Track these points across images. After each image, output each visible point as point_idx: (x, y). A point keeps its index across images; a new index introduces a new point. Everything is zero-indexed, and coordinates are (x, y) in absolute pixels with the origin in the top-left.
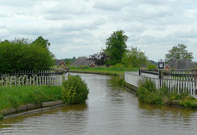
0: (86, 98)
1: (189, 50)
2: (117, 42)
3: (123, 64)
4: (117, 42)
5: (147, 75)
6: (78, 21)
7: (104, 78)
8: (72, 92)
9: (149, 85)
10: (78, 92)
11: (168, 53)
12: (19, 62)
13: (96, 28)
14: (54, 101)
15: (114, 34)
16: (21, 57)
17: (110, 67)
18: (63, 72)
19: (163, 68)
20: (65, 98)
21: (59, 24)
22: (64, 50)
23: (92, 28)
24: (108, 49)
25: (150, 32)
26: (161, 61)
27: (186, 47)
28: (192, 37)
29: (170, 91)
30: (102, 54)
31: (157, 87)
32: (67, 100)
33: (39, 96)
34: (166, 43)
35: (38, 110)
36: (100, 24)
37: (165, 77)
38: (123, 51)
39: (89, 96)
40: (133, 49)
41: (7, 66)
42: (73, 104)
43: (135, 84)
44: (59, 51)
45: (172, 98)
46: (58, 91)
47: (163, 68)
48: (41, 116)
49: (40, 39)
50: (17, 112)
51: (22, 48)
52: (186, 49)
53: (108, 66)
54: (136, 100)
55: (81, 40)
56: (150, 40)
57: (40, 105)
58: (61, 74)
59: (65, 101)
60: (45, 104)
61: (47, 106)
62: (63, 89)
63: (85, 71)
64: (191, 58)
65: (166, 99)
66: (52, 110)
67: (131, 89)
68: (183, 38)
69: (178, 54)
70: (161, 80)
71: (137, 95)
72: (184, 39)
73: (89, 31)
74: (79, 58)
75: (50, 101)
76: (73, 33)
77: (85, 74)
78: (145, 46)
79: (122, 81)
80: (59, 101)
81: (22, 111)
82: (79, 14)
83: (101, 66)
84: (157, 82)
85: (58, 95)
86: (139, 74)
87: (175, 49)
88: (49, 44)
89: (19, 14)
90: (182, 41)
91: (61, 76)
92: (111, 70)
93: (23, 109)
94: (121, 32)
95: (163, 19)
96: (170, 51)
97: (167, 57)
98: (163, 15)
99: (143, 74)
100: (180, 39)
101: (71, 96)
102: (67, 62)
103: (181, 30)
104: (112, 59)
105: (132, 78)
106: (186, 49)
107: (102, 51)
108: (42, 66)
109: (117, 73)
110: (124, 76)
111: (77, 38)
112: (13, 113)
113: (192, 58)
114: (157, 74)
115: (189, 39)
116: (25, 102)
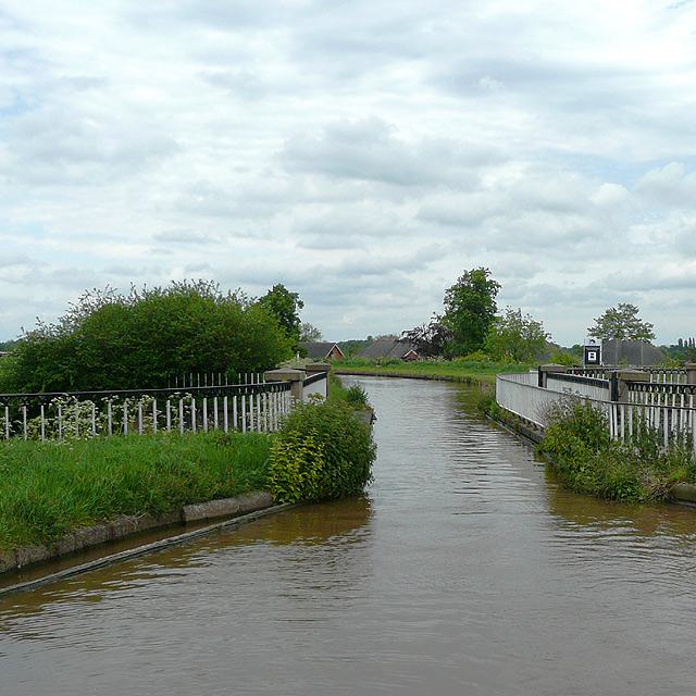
0: (365, 476)
1: (643, 317)
2: (474, 296)
3: (486, 352)
4: (474, 296)
5: (576, 388)
6: (378, 252)
7: (441, 390)
8: (309, 459)
9: (586, 427)
10: (332, 459)
11: (595, 325)
12: (183, 349)
13: (422, 268)
14: (237, 498)
15: (466, 276)
16: (188, 335)
17: (455, 360)
18: (292, 382)
19: (597, 362)
20: (278, 482)
21: (334, 259)
22: (346, 319)
23: (409, 267)
24: (450, 315)
25: (550, 275)
26: (592, 344)
27: (637, 312)
28: (645, 289)
29: (661, 442)
30: (434, 327)
31: (614, 430)
32: (288, 490)
33: (172, 478)
34: (587, 303)
35: (154, 544)
36: (432, 258)
37: (631, 395)
38: (487, 321)
39: (375, 469)
40: (512, 315)
41: (148, 362)
42: (313, 502)
43: (532, 416)
44: (326, 322)
45: (677, 476)
46: (257, 457)
47: (597, 362)
48: (184, 564)
49: (279, 289)
50: (55, 561)
51: (192, 307)
52: (636, 316)
53: (449, 358)
54: (538, 473)
55: (389, 296)
56: (549, 296)
57: (176, 518)
58: (287, 387)
59: (281, 495)
60: (196, 510)
61: (207, 521)
62: (277, 446)
63: (389, 370)
64: (648, 337)
65: (651, 480)
66: (226, 533)
67: (518, 430)
68: (627, 290)
69: (619, 328)
70: (622, 408)
71: (540, 452)
72: (628, 294)
73: (405, 276)
74: (382, 339)
75: (216, 497)
76: (365, 279)
77: (391, 381)
78: (537, 310)
79: (489, 403)
80: (259, 497)
81: (86, 551)
82: (383, 235)
83: (430, 359)
84: (609, 412)
85: (254, 473)
86: (541, 385)
87: (610, 316)
88: (301, 304)
89: (238, 235)
90: (626, 297)
91: (287, 394)
92: (456, 368)
93: (91, 540)
94: (482, 273)
95: (579, 246)
96: (599, 321)
97: (593, 335)
98: (577, 236)
99: (551, 384)
100: (621, 294)
101: (304, 476)
102: (352, 347)
103: (620, 272)
104: (460, 341)
105: (521, 396)
106: (636, 316)
107: (435, 321)
108: (254, 360)
109: (473, 376)
110: (495, 388)
111: (370, 280)
112: (33, 567)
113: (652, 336)
114: (600, 384)
115: (640, 294)
116: (100, 512)
